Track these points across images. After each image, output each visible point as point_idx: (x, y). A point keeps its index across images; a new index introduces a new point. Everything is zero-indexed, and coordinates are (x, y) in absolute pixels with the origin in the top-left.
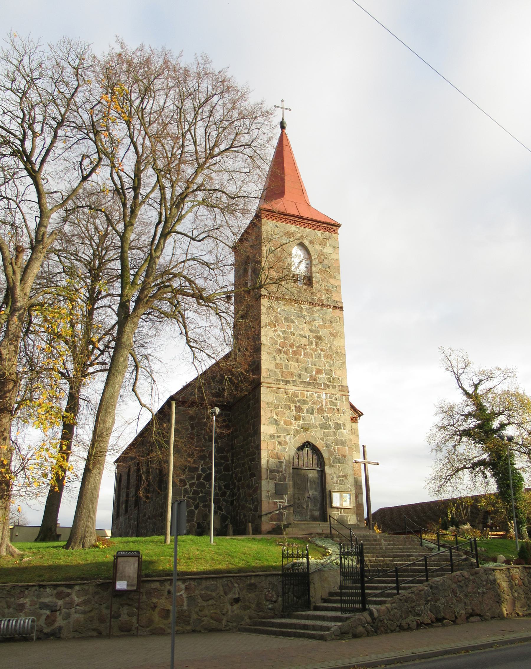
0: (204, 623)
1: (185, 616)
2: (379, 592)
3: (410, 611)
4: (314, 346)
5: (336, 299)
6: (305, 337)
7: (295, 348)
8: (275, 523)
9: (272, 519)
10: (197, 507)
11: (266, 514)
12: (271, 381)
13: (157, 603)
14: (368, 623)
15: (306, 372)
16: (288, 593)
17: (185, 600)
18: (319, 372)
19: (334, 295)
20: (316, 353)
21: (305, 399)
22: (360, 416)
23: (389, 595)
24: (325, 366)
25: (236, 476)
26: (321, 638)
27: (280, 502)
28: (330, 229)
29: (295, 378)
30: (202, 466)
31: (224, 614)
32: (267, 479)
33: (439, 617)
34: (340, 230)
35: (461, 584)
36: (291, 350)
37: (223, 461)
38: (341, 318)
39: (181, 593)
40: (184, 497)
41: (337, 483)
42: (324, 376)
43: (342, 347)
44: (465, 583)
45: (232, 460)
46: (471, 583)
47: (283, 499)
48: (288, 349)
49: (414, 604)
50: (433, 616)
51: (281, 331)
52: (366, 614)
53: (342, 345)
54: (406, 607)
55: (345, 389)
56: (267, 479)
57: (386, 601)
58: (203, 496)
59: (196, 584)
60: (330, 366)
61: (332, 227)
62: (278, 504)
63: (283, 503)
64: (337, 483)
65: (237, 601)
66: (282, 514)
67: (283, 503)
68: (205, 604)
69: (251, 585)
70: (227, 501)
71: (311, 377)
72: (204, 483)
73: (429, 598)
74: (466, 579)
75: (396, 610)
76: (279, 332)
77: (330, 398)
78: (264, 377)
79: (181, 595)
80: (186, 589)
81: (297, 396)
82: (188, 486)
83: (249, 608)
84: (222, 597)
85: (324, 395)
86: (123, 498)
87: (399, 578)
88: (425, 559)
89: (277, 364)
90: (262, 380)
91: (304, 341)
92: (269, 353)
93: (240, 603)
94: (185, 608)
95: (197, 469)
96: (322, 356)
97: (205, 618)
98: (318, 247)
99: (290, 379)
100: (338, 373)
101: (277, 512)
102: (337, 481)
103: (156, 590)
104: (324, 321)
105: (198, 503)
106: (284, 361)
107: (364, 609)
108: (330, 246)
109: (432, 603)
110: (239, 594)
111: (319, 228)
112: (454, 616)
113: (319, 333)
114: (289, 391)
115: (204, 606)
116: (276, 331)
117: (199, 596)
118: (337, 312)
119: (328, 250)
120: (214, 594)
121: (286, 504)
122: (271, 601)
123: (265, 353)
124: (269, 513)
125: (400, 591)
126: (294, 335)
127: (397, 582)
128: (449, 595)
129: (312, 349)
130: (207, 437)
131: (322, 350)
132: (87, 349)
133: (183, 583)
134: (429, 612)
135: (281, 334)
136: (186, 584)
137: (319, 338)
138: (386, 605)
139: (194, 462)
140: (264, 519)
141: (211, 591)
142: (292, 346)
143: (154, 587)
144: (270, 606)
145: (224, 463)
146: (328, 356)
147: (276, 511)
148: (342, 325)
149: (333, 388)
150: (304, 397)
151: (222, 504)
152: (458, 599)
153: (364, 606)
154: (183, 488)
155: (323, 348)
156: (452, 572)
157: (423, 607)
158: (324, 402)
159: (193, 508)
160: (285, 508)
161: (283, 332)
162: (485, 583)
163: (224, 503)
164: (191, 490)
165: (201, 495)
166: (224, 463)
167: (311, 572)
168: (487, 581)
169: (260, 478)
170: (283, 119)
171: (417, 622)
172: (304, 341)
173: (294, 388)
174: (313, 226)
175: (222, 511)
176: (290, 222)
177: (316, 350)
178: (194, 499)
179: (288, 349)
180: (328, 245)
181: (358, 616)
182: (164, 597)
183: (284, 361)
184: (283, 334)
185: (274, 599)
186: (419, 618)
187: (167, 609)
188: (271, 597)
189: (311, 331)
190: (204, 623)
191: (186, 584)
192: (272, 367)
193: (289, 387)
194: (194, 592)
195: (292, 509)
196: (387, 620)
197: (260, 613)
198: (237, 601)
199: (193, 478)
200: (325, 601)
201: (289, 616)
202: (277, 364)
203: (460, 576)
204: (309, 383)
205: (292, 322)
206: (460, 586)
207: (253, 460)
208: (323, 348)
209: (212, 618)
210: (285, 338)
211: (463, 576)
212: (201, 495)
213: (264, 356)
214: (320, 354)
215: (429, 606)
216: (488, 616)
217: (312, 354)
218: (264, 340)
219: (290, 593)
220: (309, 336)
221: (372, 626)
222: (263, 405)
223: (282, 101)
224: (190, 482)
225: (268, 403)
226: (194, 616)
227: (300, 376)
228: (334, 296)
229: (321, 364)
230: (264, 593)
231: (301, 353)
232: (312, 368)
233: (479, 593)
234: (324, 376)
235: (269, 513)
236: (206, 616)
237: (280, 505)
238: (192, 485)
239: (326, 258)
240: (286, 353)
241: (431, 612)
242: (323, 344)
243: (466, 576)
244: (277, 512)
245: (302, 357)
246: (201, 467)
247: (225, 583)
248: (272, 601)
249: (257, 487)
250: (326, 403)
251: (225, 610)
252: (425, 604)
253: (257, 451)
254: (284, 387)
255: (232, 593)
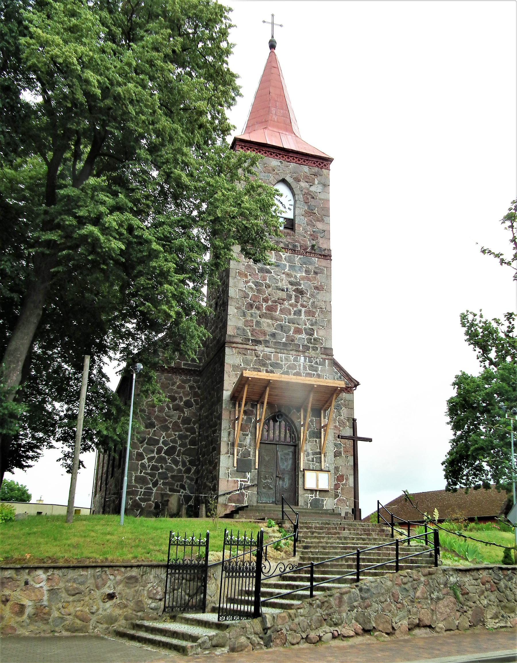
0: (67, 622)
1: (44, 614)
2: (288, 591)
3: (325, 620)
4: (293, 301)
5: (324, 246)
6: (283, 290)
7: (270, 303)
8: (234, 504)
9: (230, 500)
10: (155, 484)
11: (224, 495)
12: (239, 340)
13: (10, 595)
14: (256, 633)
15: (282, 331)
16: (177, 590)
17: (45, 592)
18: (298, 331)
19: (321, 241)
20: (295, 309)
21: (279, 362)
22: (356, 386)
23: (301, 598)
24: (306, 325)
25: (201, 450)
26: (181, 650)
27: (241, 481)
28: (320, 164)
29: (268, 338)
30: (164, 438)
31: (93, 613)
32: (227, 453)
33: (367, 627)
34: (332, 166)
35: (406, 586)
36: (264, 305)
37: (189, 433)
38: (329, 268)
39: (41, 585)
40: (141, 473)
41: (313, 461)
42: (304, 336)
43: (328, 302)
44: (412, 586)
45: (199, 433)
46: (422, 586)
47: (245, 477)
48: (261, 303)
49: (331, 611)
50: (359, 627)
51: (253, 282)
52: (257, 622)
53: (327, 299)
54: (319, 614)
55: (328, 352)
56: (227, 453)
57: (292, 605)
58: (163, 473)
59: (61, 574)
60: (312, 325)
61: (323, 161)
62: (239, 483)
63: (245, 482)
64: (313, 461)
65: (111, 596)
66: (243, 494)
67: (245, 482)
68: (71, 599)
69: (130, 578)
70: (191, 479)
71: (288, 337)
72: (165, 458)
73: (355, 604)
74: (414, 580)
75: (302, 618)
76: (251, 284)
77: (309, 362)
78: (230, 336)
79: (41, 587)
80: (48, 579)
81: (270, 359)
82: (146, 460)
83: (126, 606)
84: (92, 592)
85: (302, 358)
86: (100, 475)
87: (356, 577)
88: (358, 554)
89: (247, 321)
90: (227, 339)
91: (283, 295)
92: (237, 308)
93: (115, 600)
94: (45, 603)
95: (157, 442)
96: (303, 312)
97: (68, 617)
98: (303, 184)
99: (261, 339)
100: (322, 333)
101: (238, 492)
102: (313, 459)
103: (10, 579)
104: (307, 272)
105: (157, 481)
106: (256, 318)
107: (257, 614)
108: (318, 184)
109: (360, 610)
110: (114, 588)
111: (307, 162)
112: (390, 627)
113: (300, 286)
114: (259, 352)
115: (68, 602)
116: (247, 282)
117: (63, 589)
118: (324, 263)
119: (316, 188)
120: (82, 588)
121: (249, 483)
122: (154, 599)
123: (232, 307)
124: (227, 494)
125: (314, 593)
126: (269, 287)
127: (311, 579)
128: (386, 601)
129: (291, 305)
130: (171, 406)
131: (303, 306)
132: (124, 317)
133: (44, 573)
134: (353, 621)
135: (253, 286)
136: (49, 574)
137: (301, 292)
138: (289, 611)
139: (154, 434)
140: (221, 500)
141: (79, 584)
142: (266, 300)
143: (9, 576)
144: (153, 605)
145: (190, 436)
146: (309, 313)
147: (236, 491)
148: (329, 277)
149: (314, 350)
150: (278, 360)
151: (185, 482)
152: (399, 605)
153: (257, 609)
154: (140, 462)
155: (305, 303)
156: (397, 570)
157: (344, 615)
158: (302, 366)
159: (151, 486)
160: (247, 488)
161: (257, 284)
162: (442, 586)
163: (188, 481)
164: (149, 466)
165: (161, 471)
166: (190, 436)
167: (209, 563)
168: (445, 585)
169: (219, 453)
170: (273, 37)
171: (333, 634)
172: (283, 295)
173: (266, 349)
174: (299, 160)
175: (185, 489)
176: (271, 154)
177: (296, 306)
178: (152, 475)
179: (261, 303)
180: (316, 182)
181: (246, 622)
182: (18, 589)
183: (256, 318)
184: (255, 286)
185: (158, 597)
186: (336, 629)
187: (22, 603)
188: (155, 594)
189: (291, 283)
190: (67, 622)
191: (49, 574)
192: (240, 324)
193: (259, 348)
194: (57, 585)
195: (255, 489)
196: (287, 630)
197: (139, 614)
198: (111, 596)
199: (153, 452)
200: (232, 601)
201: (174, 618)
202: (247, 321)
203: (405, 576)
204: (285, 344)
205: (267, 272)
206: (405, 589)
207: (214, 432)
208: (305, 303)
209: (77, 617)
210: (259, 291)
211: (411, 577)
212: (161, 471)
213: (232, 310)
214: (300, 311)
215: (354, 613)
216: (441, 628)
217: (290, 310)
218: (232, 292)
219: (180, 590)
220: (287, 289)
221: (261, 638)
222: (227, 368)
223: (273, 15)
224: (149, 456)
225: (234, 366)
226: (56, 614)
227: (273, 335)
228: (321, 242)
229: (301, 322)
230: (146, 588)
231: (277, 309)
232: (289, 327)
233: (432, 599)
234: (304, 336)
235: (227, 494)
236: (69, 615)
237: (241, 485)
238: (150, 459)
239: (313, 198)
240: (258, 308)
241: (357, 621)
242: (305, 299)
243: (415, 577)
244: (238, 492)
245: (278, 313)
246: (162, 440)
247: (98, 574)
248: (156, 599)
249: (216, 463)
250: (305, 368)
251: (95, 607)
252: (349, 611)
253: (219, 422)
254: (253, 347)
255: (106, 587)
